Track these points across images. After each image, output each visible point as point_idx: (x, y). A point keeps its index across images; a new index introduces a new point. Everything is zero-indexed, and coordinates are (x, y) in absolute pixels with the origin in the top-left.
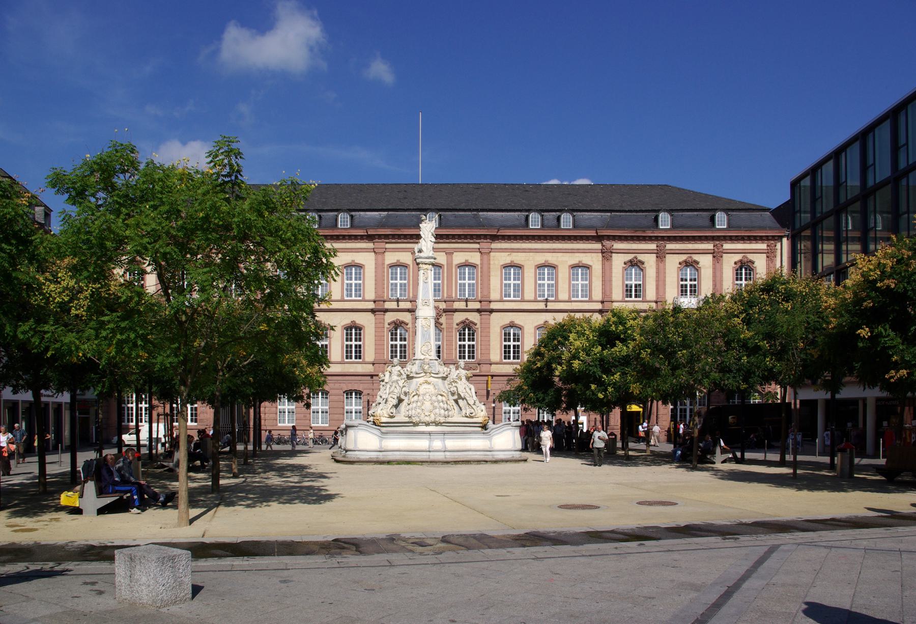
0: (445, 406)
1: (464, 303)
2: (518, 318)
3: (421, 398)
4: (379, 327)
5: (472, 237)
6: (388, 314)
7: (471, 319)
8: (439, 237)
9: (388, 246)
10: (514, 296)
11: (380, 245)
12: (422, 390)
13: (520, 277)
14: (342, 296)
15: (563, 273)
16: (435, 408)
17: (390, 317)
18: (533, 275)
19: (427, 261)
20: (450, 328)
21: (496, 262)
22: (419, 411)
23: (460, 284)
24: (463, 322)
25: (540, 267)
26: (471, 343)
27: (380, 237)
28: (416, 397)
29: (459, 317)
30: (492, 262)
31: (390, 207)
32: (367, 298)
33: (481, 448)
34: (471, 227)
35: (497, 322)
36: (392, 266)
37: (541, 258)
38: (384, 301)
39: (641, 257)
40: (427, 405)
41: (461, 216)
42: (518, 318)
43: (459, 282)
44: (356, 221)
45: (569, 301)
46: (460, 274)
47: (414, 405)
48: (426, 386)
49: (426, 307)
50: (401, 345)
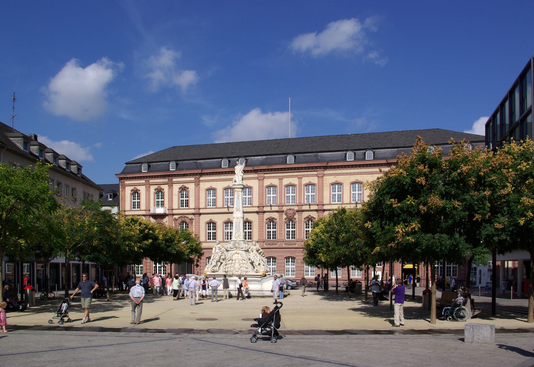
0: (246, 266)
1: (308, 206)
2: (214, 218)
3: (233, 262)
4: (261, 221)
5: (312, 168)
6: (266, 214)
7: (312, 215)
8: (245, 172)
9: (266, 175)
10: (338, 201)
11: (261, 175)
12: (234, 258)
13: (215, 195)
14: (330, 201)
15: (220, 192)
16: (241, 267)
17: (267, 216)
18: (349, 188)
19: (239, 186)
20: (300, 221)
21: (327, 182)
22: (232, 268)
23: (353, 194)
24: (308, 217)
25: (353, 183)
26: (274, 230)
27: (261, 170)
28: (230, 262)
29: (305, 215)
30: (324, 182)
31: (268, 153)
32: (254, 205)
33: (257, 289)
34: (312, 162)
35: (204, 219)
36: (268, 187)
37: (353, 178)
38: (263, 207)
39: (187, 185)
40: (237, 265)
41: (160, 165)
42: (214, 218)
43: (286, 195)
44: (249, 163)
45: (330, 204)
46: (333, 188)
47: (230, 265)
48: (236, 255)
49: (238, 212)
50: (273, 232)
